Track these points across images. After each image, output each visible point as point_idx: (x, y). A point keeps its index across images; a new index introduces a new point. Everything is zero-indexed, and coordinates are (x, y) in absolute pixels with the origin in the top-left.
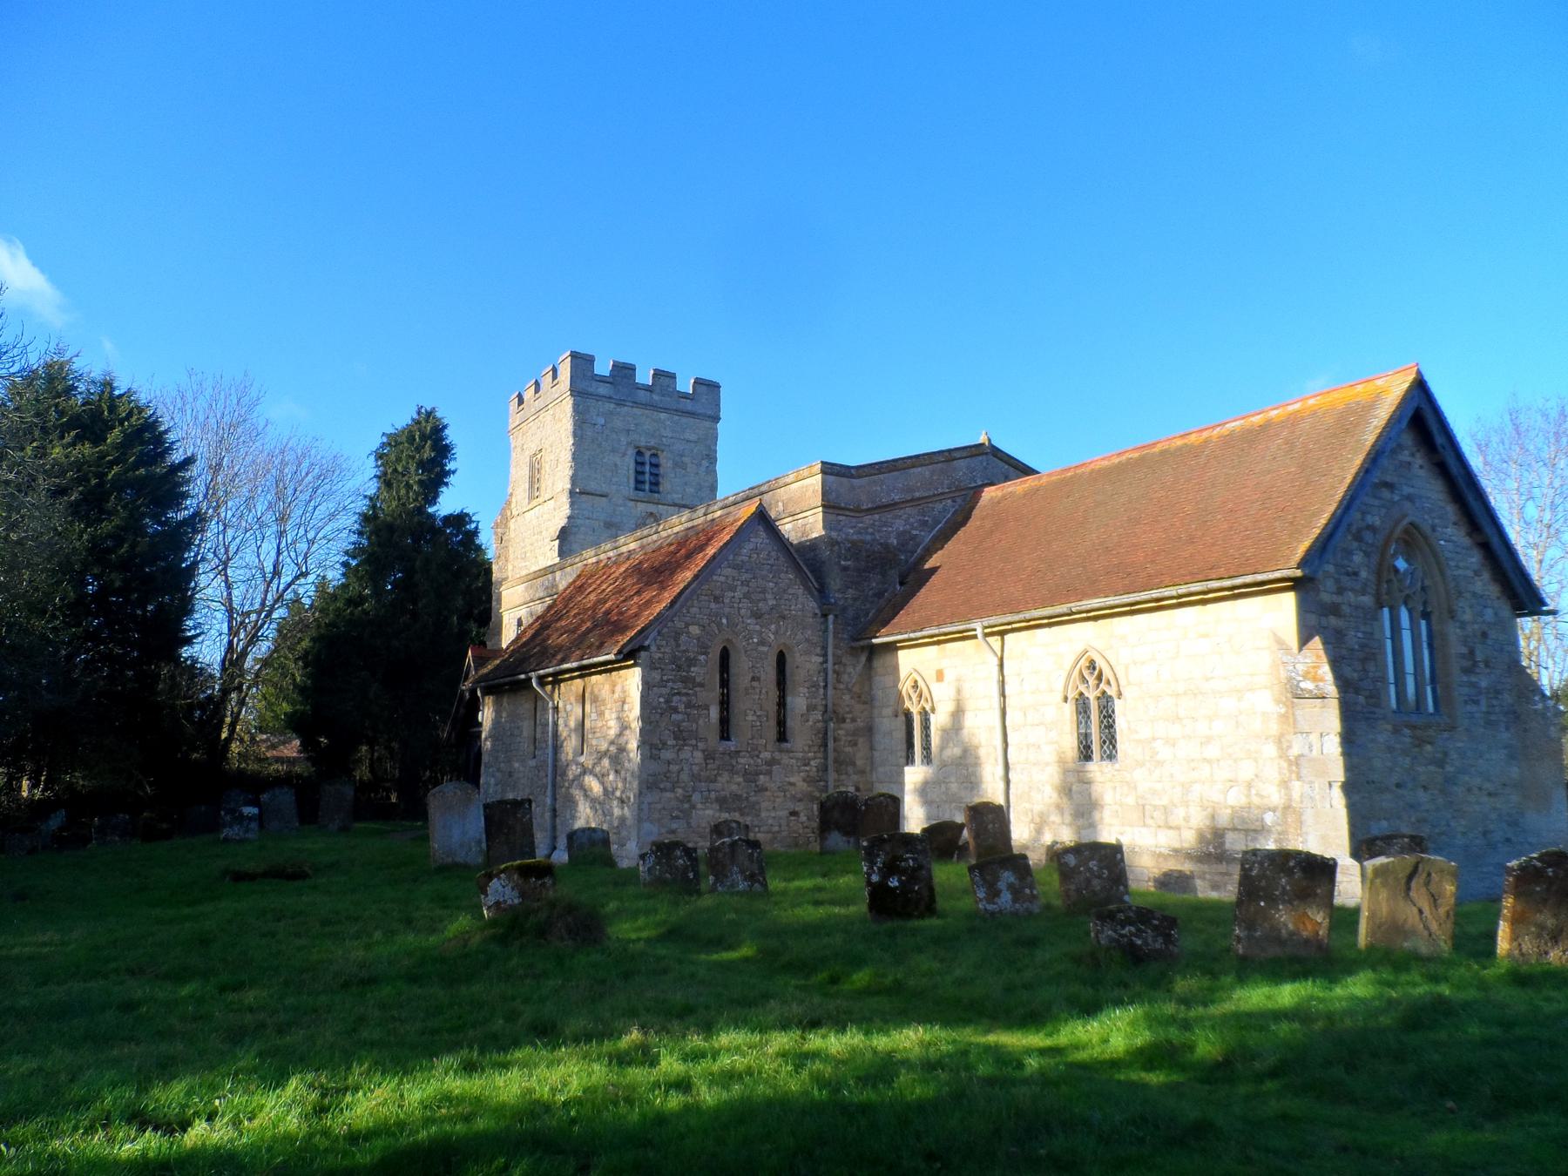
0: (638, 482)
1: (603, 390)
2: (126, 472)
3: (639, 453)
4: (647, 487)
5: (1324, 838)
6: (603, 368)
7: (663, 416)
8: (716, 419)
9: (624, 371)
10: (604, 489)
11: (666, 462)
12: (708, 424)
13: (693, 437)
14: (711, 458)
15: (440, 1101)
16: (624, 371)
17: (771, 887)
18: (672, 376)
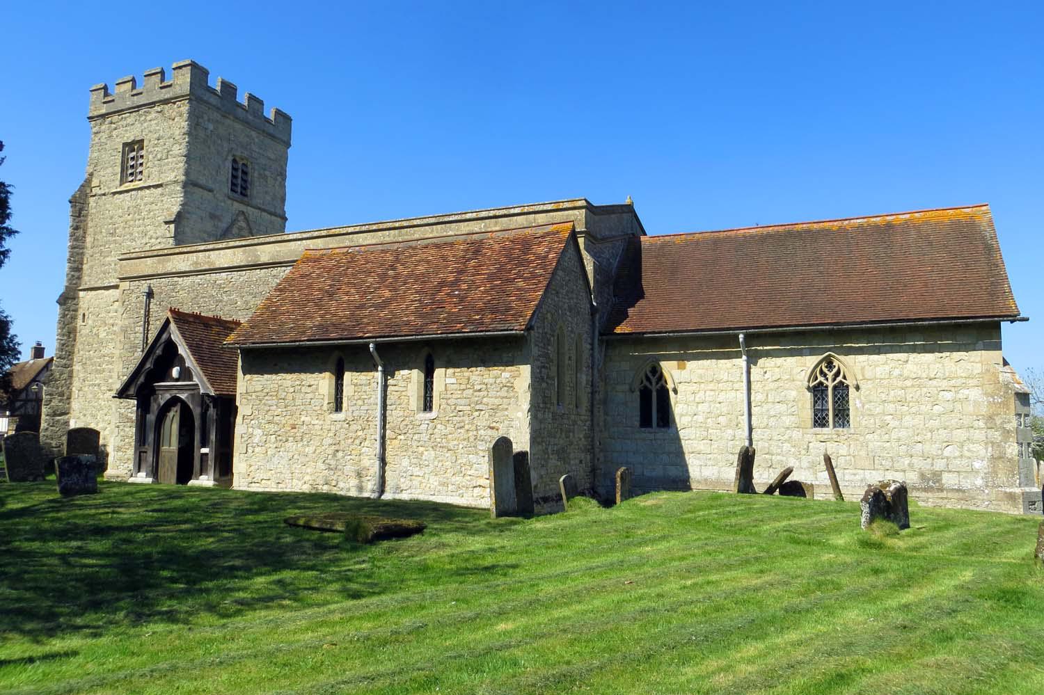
0: (233, 184)
1: (213, 100)
2: (221, 490)
3: (234, 161)
4: (239, 190)
5: (526, 381)
6: (215, 83)
7: (254, 134)
8: (288, 145)
9: (229, 89)
10: (211, 185)
11: (254, 175)
12: (280, 147)
13: (273, 157)
14: (283, 175)
15: (238, 215)
16: (229, 89)
17: (815, 498)
18: (261, 103)
